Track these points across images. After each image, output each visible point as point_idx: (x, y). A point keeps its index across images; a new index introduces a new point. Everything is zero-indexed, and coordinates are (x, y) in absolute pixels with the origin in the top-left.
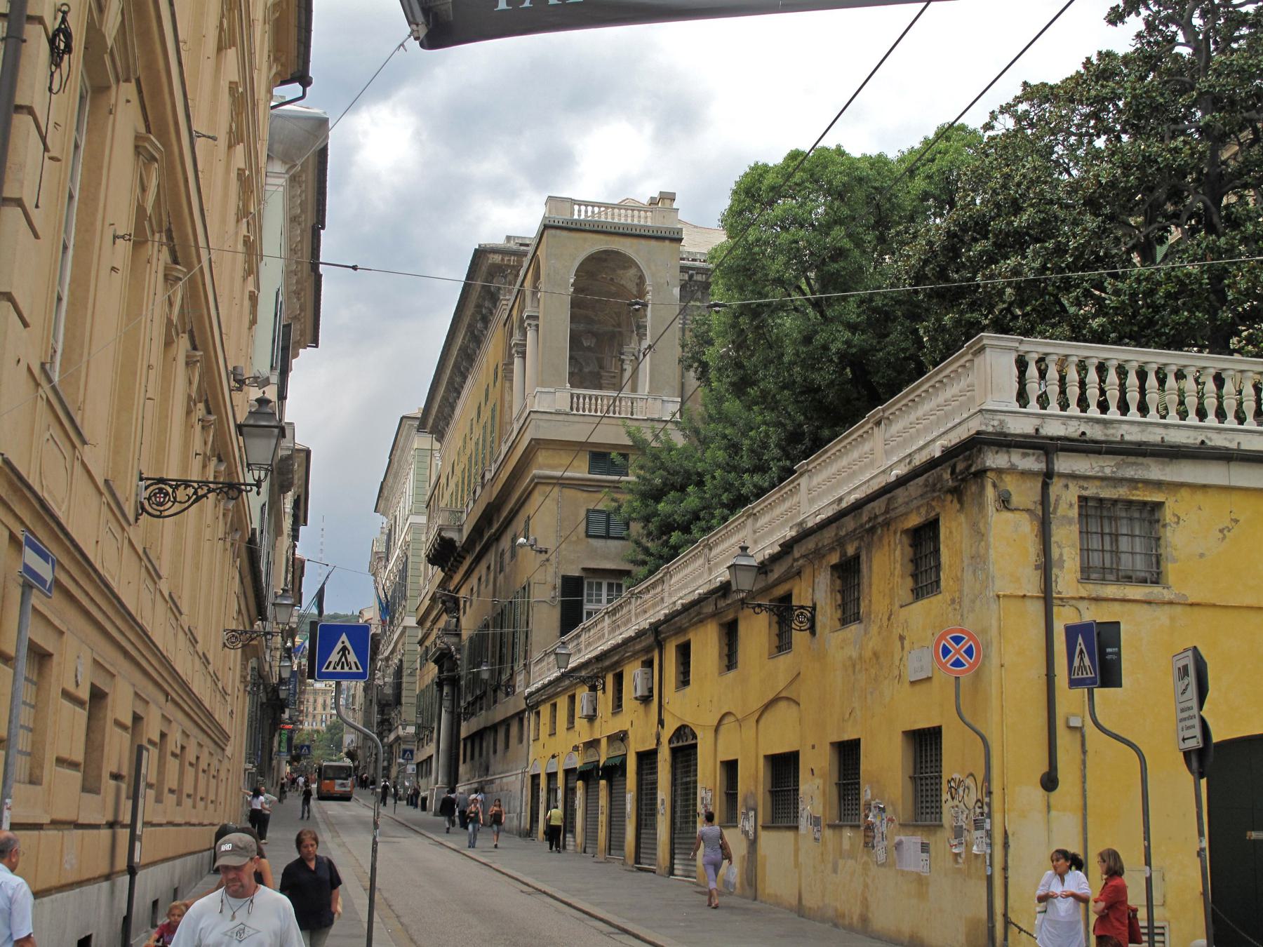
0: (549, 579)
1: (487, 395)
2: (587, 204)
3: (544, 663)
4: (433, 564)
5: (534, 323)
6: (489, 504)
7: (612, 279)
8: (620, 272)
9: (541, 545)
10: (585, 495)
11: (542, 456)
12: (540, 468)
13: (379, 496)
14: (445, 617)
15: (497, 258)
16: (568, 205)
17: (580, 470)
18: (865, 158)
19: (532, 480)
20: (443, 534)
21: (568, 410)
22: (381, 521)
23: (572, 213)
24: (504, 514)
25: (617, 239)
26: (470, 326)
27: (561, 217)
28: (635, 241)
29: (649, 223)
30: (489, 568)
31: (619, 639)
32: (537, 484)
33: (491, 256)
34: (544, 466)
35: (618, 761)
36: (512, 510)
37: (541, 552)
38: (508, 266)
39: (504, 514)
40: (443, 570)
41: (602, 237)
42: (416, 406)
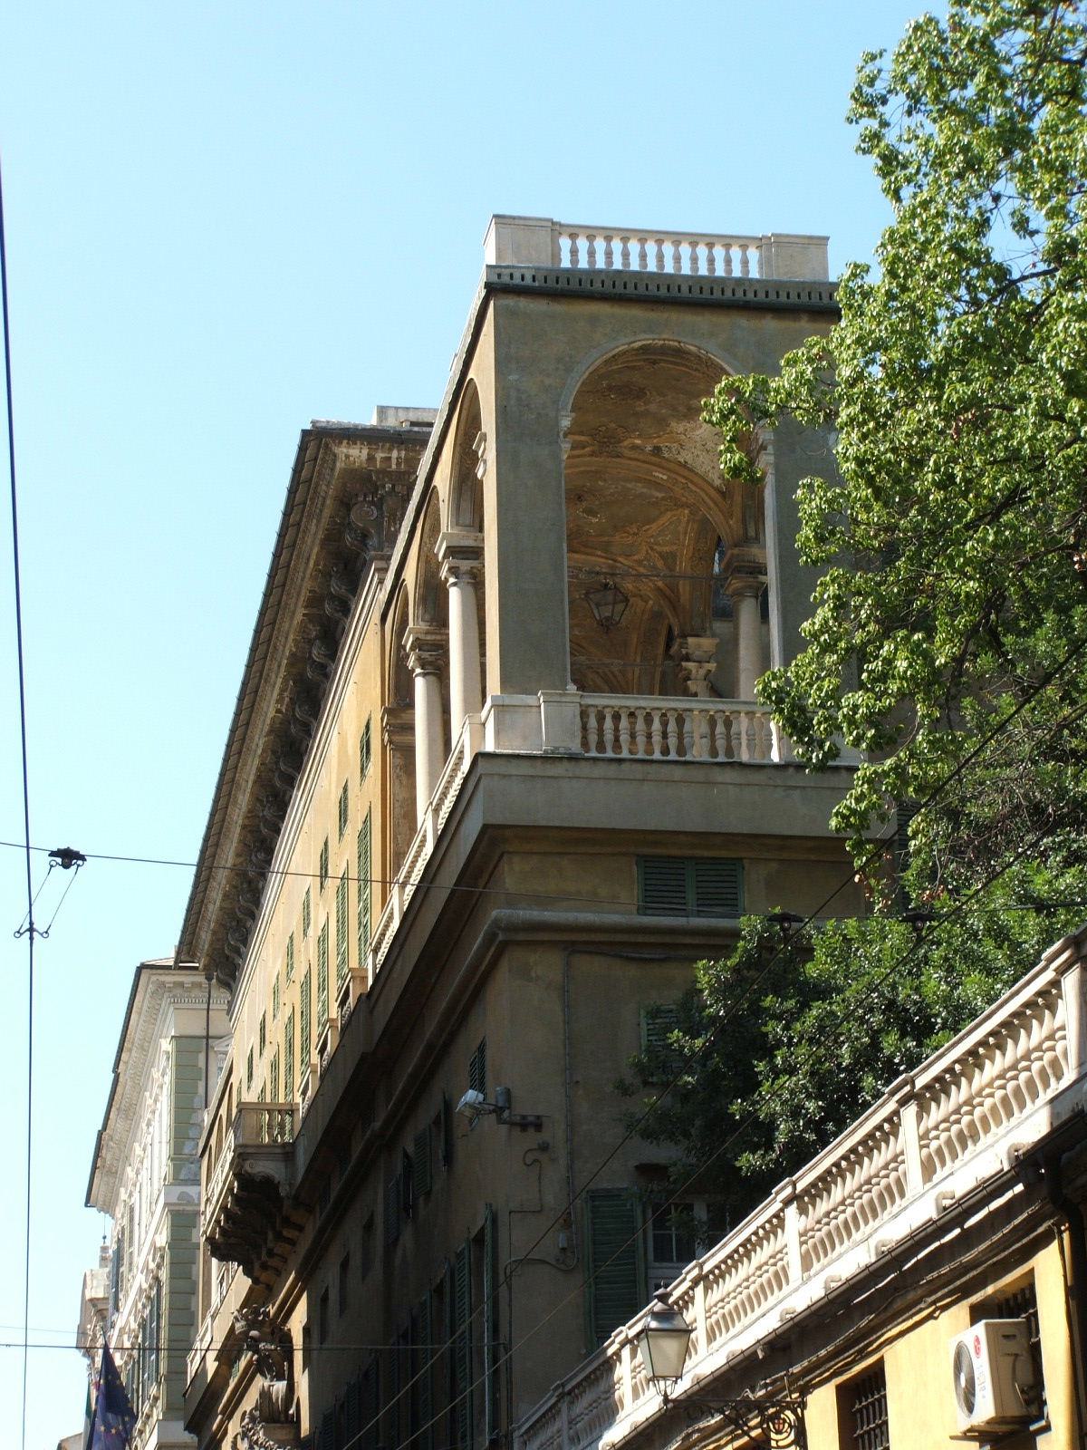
0: (549, 1199)
1: (290, 954)
2: (591, 233)
3: (561, 1422)
4: (222, 1258)
5: (465, 565)
6: (363, 1058)
7: (657, 450)
8: (678, 427)
9: (523, 1108)
10: (633, 971)
11: (513, 875)
12: (512, 901)
13: (94, 1168)
14: (260, 1382)
15: (357, 454)
16: (545, 237)
17: (615, 904)
18: (989, 1423)
19: (491, 937)
20: (247, 1167)
21: (576, 747)
22: (101, 1227)
23: (556, 255)
24: (430, 1028)
25: (674, 316)
26: (294, 660)
27: (528, 261)
28: (722, 320)
29: (754, 273)
30: (369, 1227)
31: (851, 1260)
32: (504, 947)
33: (342, 450)
34: (521, 894)
35: (1024, 1284)
36: (430, 1047)
37: (524, 1126)
38: (384, 473)
39: (430, 1028)
40: (247, 1273)
41: (636, 312)
42: (163, 945)
